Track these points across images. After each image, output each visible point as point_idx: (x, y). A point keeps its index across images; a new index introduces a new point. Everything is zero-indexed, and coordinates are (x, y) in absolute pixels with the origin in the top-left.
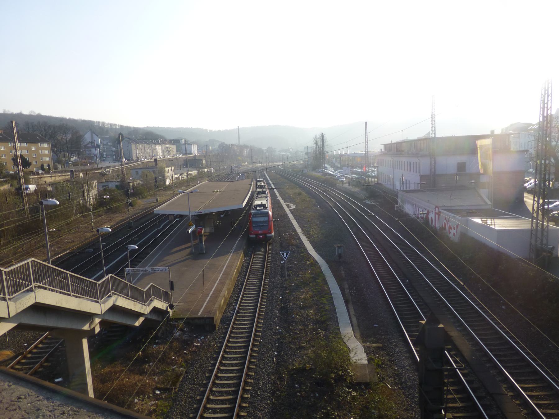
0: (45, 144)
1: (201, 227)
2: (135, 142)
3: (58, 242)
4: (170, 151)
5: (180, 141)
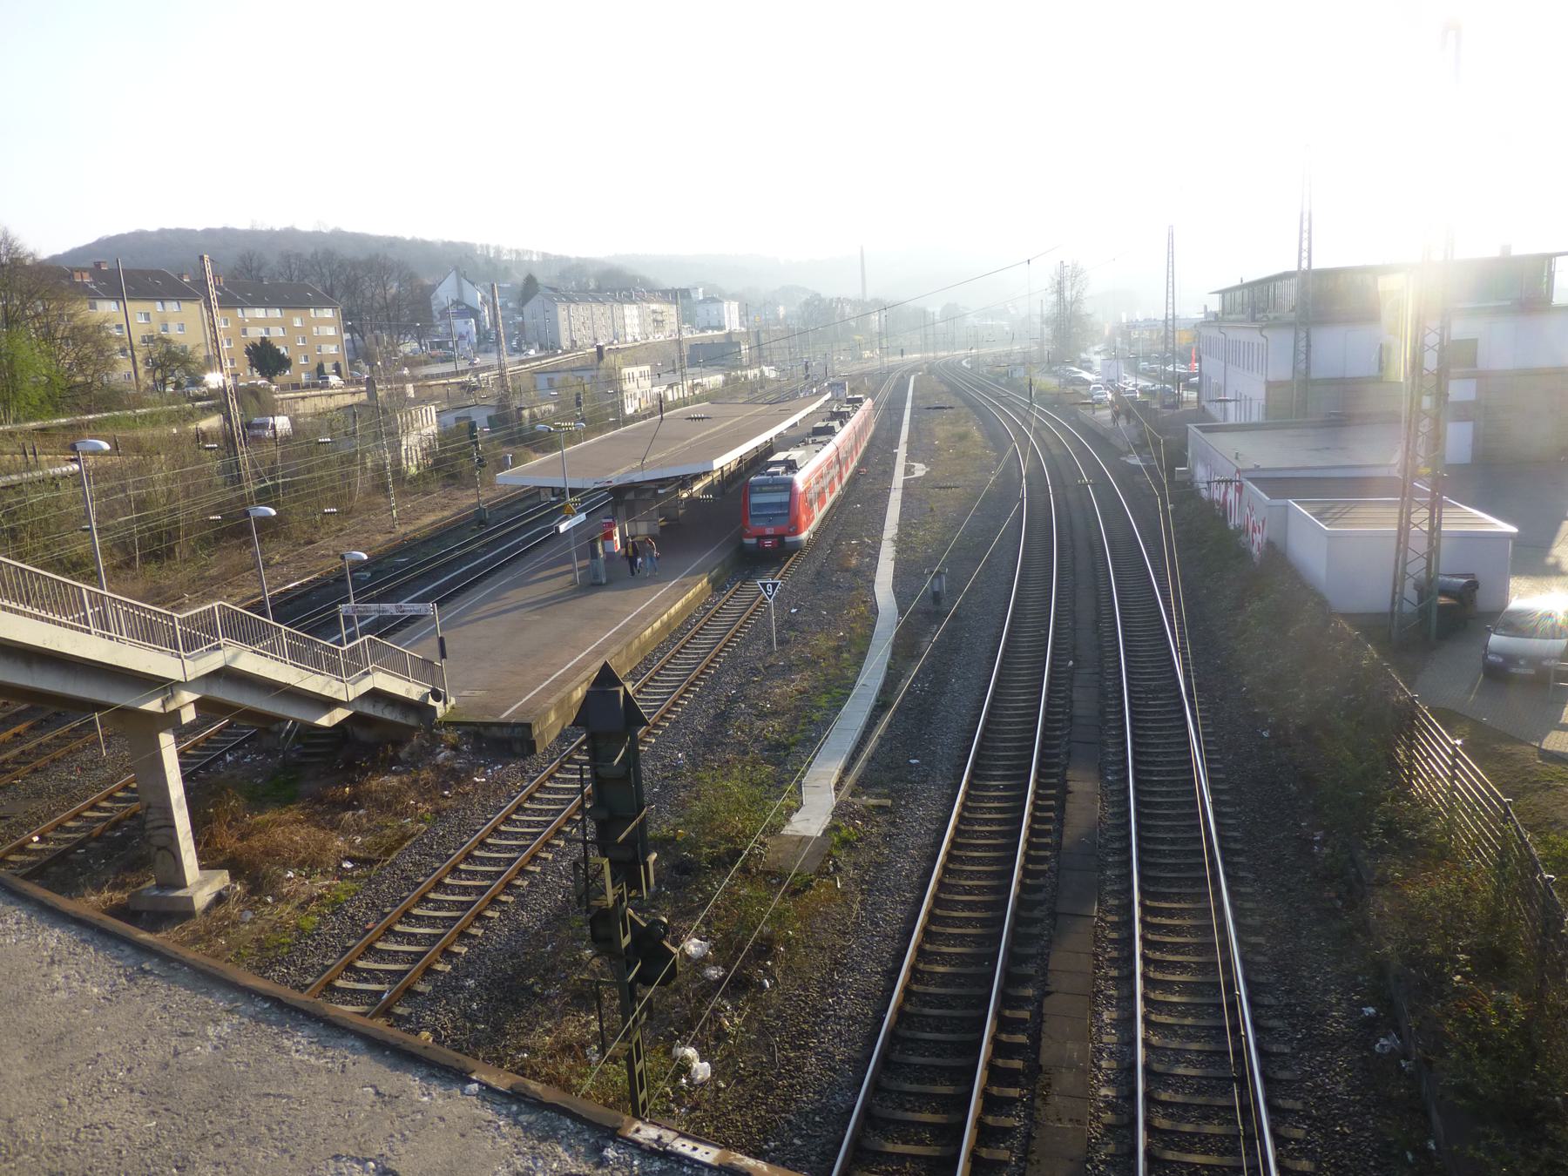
0: (257, 310)
1: (611, 520)
2: (567, 298)
3: (301, 556)
4: (662, 321)
5: (689, 293)
